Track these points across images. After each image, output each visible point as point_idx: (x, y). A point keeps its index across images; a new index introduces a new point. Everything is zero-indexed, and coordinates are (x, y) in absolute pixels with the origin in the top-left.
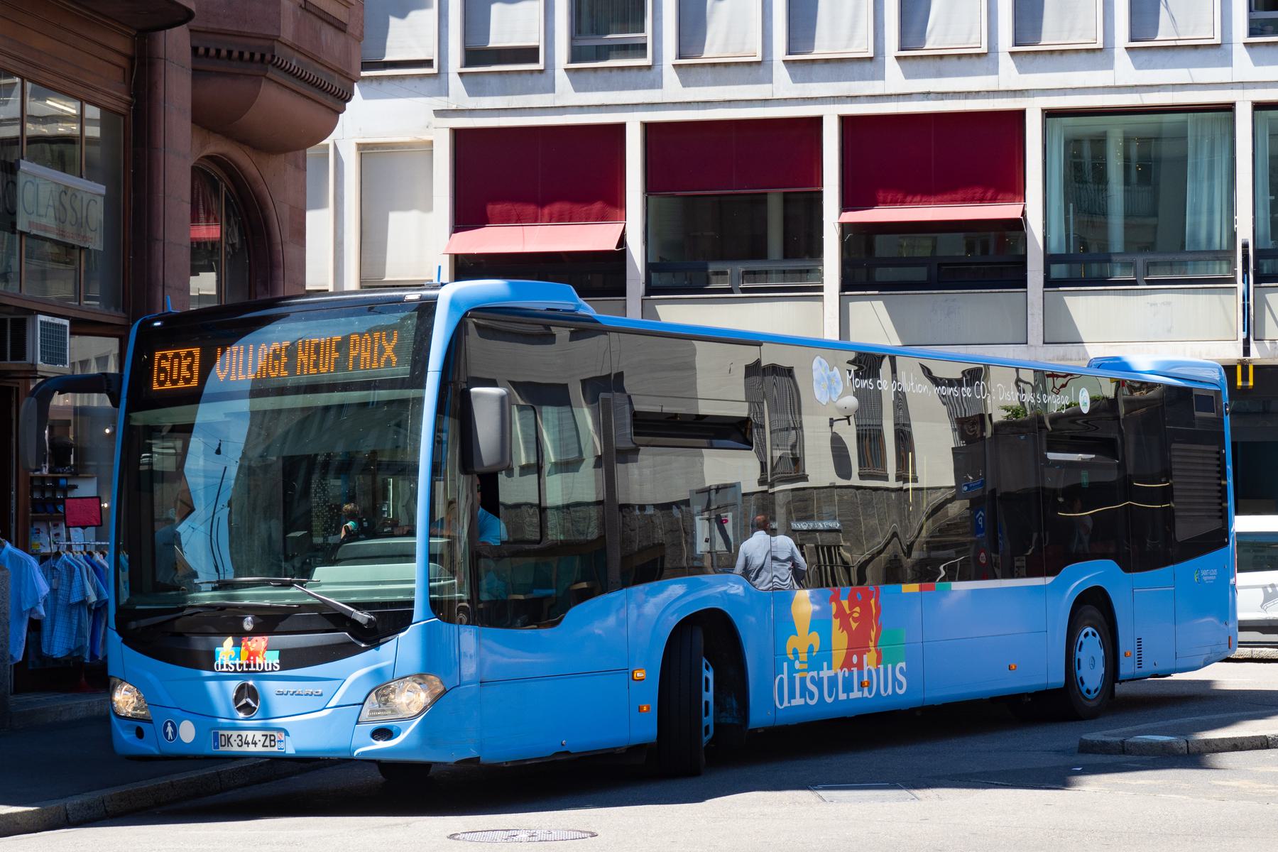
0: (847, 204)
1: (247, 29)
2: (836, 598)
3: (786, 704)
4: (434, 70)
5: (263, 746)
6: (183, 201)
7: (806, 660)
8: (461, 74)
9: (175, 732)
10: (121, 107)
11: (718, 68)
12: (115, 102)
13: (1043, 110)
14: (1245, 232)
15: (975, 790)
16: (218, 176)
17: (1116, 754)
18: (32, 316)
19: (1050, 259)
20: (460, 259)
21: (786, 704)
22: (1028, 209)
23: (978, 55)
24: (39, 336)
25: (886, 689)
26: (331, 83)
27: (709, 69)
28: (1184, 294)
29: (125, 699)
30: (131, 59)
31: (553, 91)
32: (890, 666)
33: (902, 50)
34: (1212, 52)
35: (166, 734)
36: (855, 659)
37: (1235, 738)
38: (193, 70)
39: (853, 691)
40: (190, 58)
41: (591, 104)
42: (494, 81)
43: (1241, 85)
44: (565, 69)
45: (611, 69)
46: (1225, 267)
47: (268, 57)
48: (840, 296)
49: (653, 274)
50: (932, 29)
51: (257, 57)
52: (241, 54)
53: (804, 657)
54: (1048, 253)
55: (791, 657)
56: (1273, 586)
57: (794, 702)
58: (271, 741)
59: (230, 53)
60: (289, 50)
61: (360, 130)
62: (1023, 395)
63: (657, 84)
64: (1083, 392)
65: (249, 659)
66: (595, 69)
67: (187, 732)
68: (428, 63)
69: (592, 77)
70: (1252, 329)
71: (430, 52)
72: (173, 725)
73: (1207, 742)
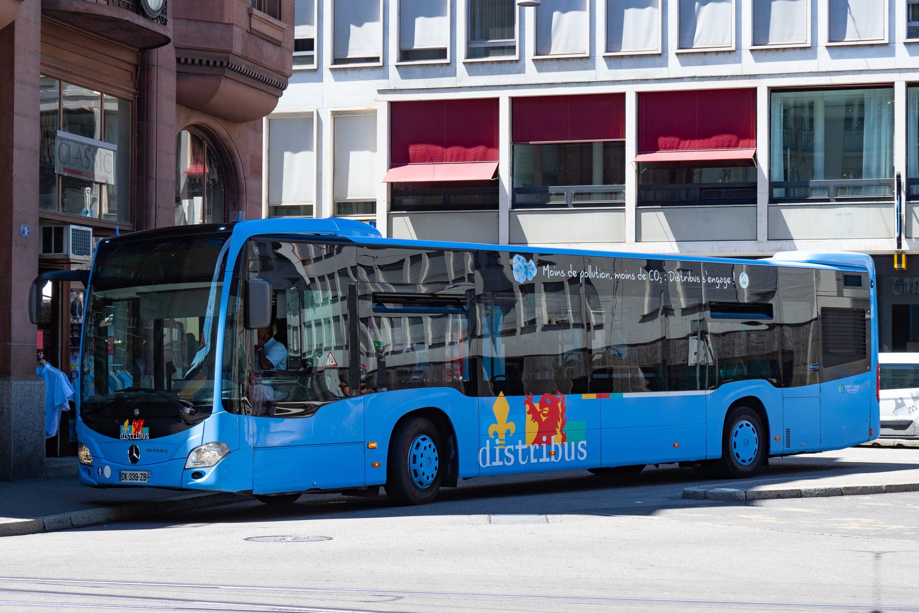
0: (642, 149)
1: (212, 47)
2: (529, 402)
3: (488, 464)
4: (380, 64)
5: (141, 480)
6: (170, 154)
7: (504, 439)
8: (397, 66)
9: (102, 472)
10: (130, 96)
11: (561, 61)
12: (125, 93)
13: (769, 88)
14: (900, 167)
15: (593, 516)
16: (203, 138)
17: (701, 499)
18: (66, 226)
19: (772, 185)
20: (394, 186)
21: (488, 464)
22: (758, 152)
23: (729, 52)
24: (71, 238)
25: (569, 456)
26: (271, 79)
27: (555, 62)
28: (860, 207)
29: (84, 453)
30: (136, 66)
31: (456, 76)
32: (573, 443)
33: (680, 49)
34: (882, 49)
35: (99, 473)
36: (544, 439)
37: (779, 491)
38: (177, 72)
39: (542, 458)
40: (175, 65)
41: (500, 84)
42: (418, 70)
43: (898, 70)
44: (464, 63)
45: (492, 62)
46: (887, 190)
47: (225, 64)
48: (636, 209)
49: (517, 195)
50: (699, 36)
51: (218, 63)
52: (208, 62)
53: (503, 437)
54: (772, 181)
55: (492, 437)
56: (901, 399)
57: (494, 464)
58: (144, 477)
59: (201, 61)
60: (241, 59)
61: (333, 102)
62: (690, 278)
63: (522, 71)
64: (742, 275)
65: (135, 433)
66: (483, 63)
67: (108, 472)
68: (376, 59)
69: (480, 67)
70: (904, 229)
71: (377, 52)
72: (102, 468)
73: (760, 493)
